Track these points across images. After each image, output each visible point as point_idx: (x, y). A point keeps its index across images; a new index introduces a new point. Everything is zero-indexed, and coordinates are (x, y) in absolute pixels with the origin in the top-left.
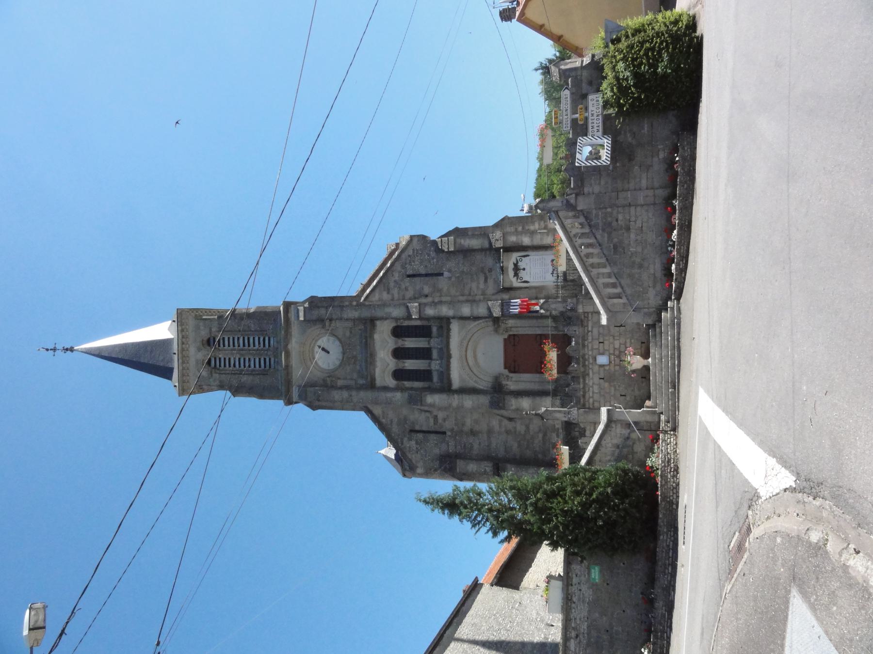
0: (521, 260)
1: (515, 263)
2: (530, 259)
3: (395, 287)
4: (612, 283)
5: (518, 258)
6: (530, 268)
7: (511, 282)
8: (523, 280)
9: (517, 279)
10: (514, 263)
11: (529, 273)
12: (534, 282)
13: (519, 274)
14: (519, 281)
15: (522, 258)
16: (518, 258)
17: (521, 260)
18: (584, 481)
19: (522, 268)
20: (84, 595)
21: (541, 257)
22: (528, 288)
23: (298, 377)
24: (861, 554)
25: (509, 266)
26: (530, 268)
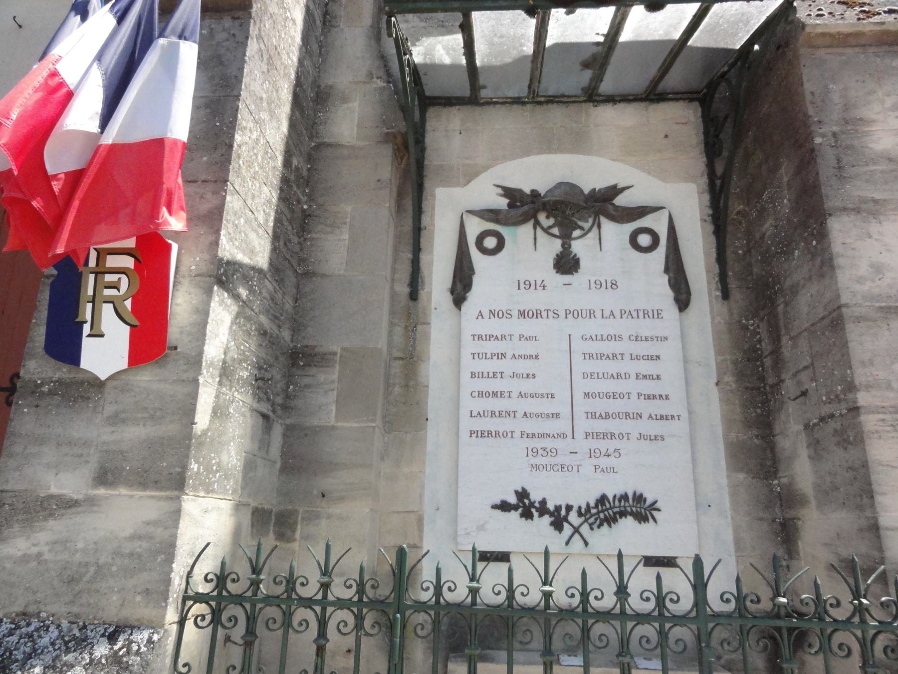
0: (644, 240)
1: (621, 200)
2: (658, 314)
3: (167, 656)
4: (285, 436)
5: (660, 226)
6: (577, 314)
7: (470, 175)
8: (629, 227)
9: (491, 215)
10: (614, 191)
11: (533, 300)
12: (458, 338)
13: (526, 230)
14: (474, 227)
15: (661, 251)
16: (660, 226)
17: (644, 240)
18: (348, 224)
19: (578, 247)
20: (338, 558)
21: (676, 406)
22: (414, 295)
23: (167, 240)
24: (218, 182)
25: (595, 160)
26: (577, 314)
